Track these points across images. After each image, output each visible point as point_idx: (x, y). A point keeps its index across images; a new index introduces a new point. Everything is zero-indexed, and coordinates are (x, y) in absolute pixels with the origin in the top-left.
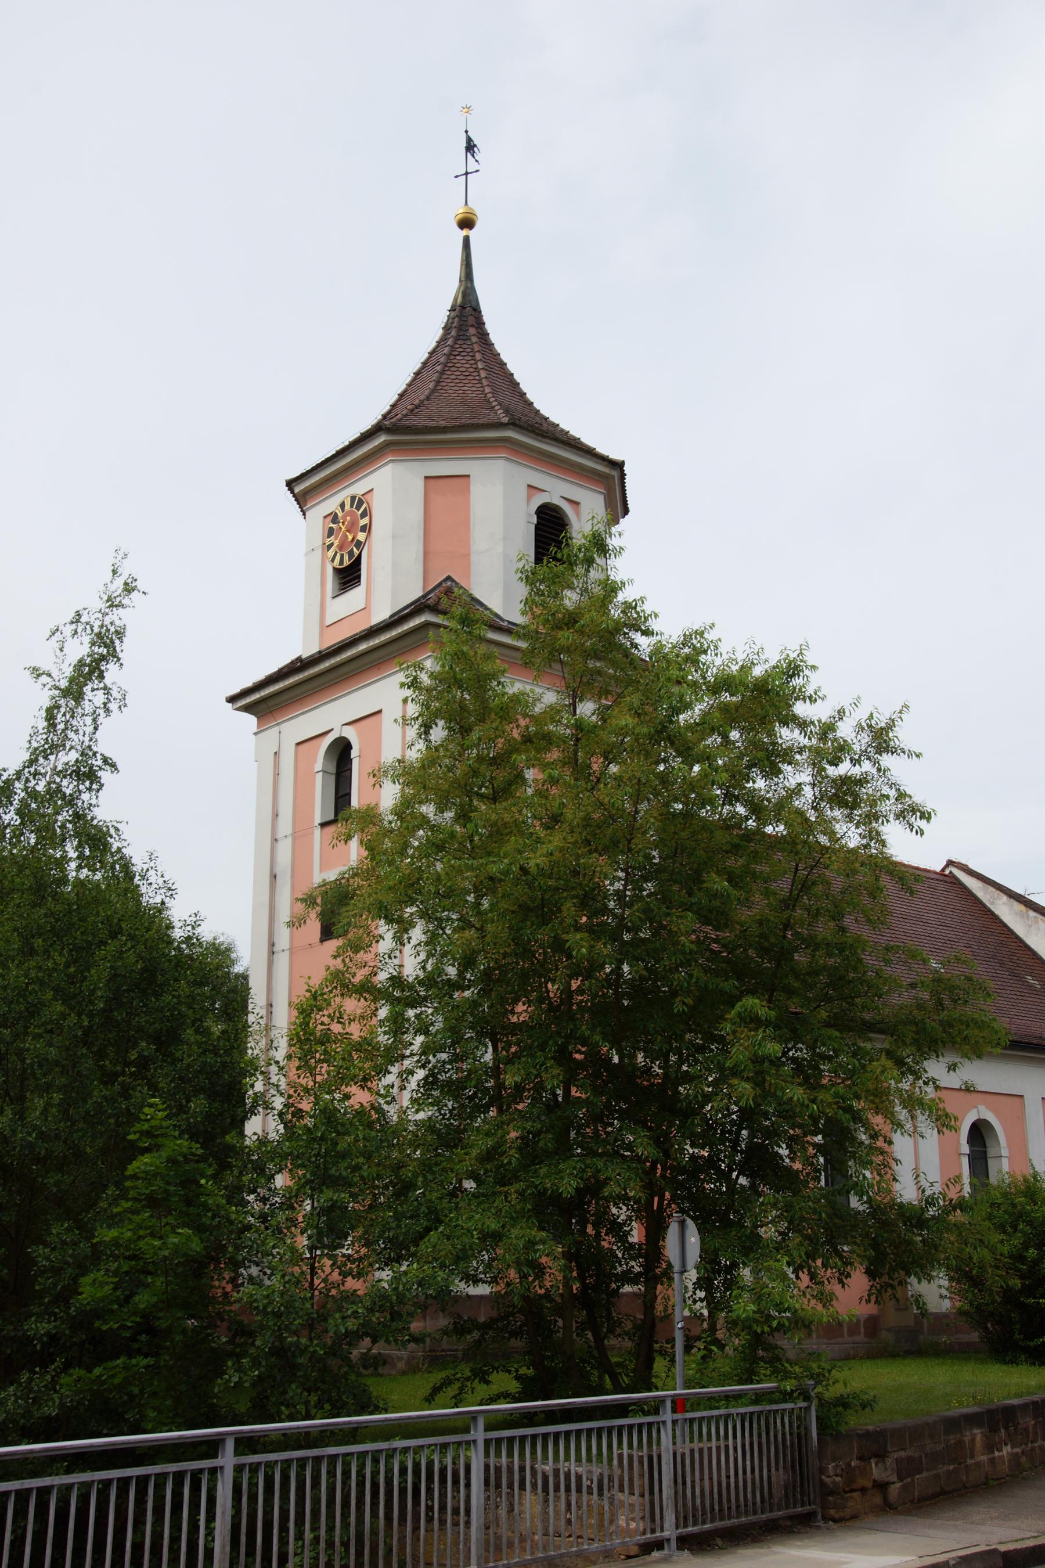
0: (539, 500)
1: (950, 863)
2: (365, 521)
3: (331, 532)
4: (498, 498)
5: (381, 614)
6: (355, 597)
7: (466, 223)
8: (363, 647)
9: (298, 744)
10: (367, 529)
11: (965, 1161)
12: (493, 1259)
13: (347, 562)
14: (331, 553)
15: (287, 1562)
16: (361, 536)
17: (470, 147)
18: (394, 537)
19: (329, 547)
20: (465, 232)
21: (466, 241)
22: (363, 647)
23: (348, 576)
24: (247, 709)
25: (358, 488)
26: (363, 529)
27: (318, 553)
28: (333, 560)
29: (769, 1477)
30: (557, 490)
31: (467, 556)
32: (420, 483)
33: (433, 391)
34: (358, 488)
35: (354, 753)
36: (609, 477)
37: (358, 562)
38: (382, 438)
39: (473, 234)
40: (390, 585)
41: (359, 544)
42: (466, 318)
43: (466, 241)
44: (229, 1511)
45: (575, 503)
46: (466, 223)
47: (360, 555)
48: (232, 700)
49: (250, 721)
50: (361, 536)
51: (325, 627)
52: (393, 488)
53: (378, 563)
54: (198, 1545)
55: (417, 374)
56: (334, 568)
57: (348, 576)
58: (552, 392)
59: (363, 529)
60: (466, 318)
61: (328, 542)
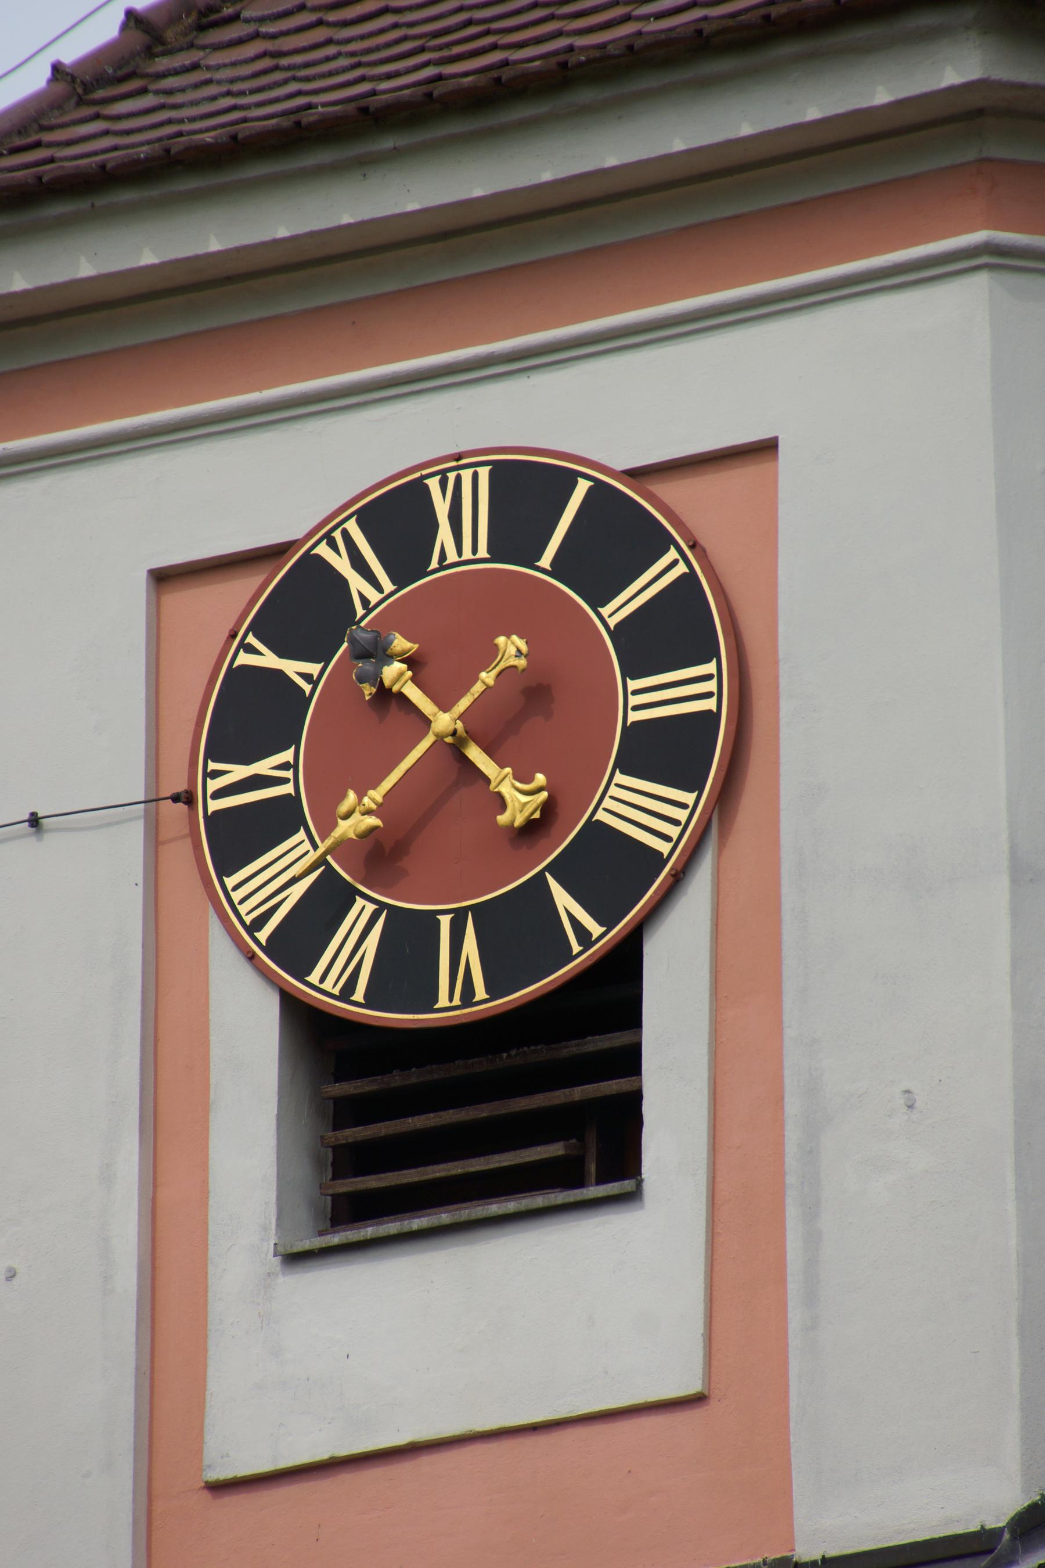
2: (682, 692)
3: (251, 715)
6: (537, 1314)
9: (163, 578)
13: (462, 984)
14: (279, 877)
16: (638, 808)
18: (1022, 873)
19: (241, 836)
25: (610, 407)
26: (668, 751)
27: (107, 873)
28: (299, 940)
34: (610, 407)
41: (614, 870)
44: (242, 57)
47: (623, 965)
50: (638, 808)
54: (146, 412)
56: (310, 1028)
59: (668, 751)
61: (227, 784)
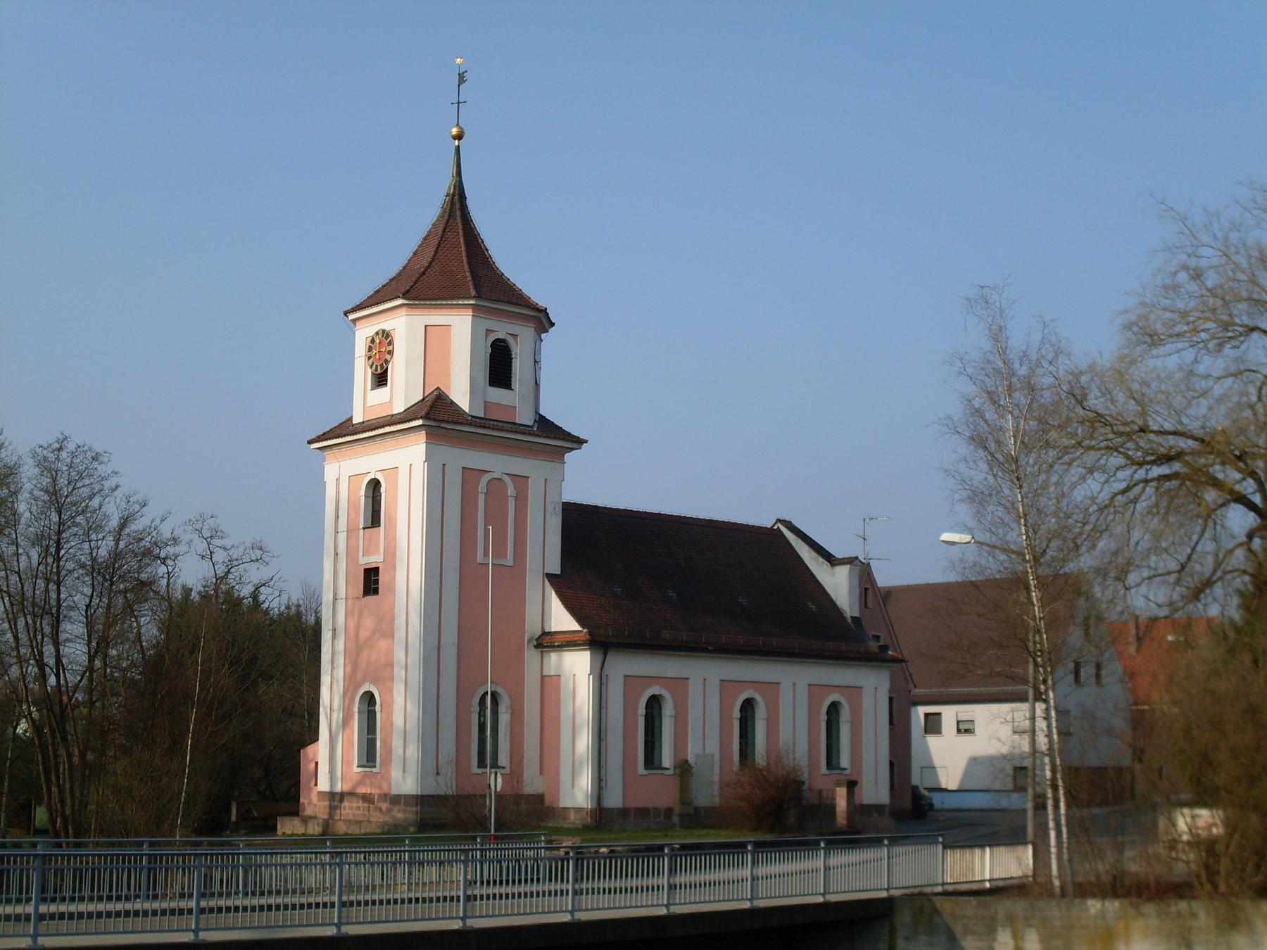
0: (492, 338)
1: (779, 521)
2: (390, 348)
5: (399, 408)
6: (383, 392)
10: (391, 353)
13: (379, 371)
15: (314, 738)
16: (388, 357)
20: (457, 143)
21: (458, 148)
29: (74, 882)
30: (502, 329)
35: (383, 490)
36: (541, 321)
42: (457, 203)
43: (458, 148)
45: (515, 336)
50: (388, 357)
53: (398, 370)
55: (425, 239)
58: (508, 259)
60: (457, 203)
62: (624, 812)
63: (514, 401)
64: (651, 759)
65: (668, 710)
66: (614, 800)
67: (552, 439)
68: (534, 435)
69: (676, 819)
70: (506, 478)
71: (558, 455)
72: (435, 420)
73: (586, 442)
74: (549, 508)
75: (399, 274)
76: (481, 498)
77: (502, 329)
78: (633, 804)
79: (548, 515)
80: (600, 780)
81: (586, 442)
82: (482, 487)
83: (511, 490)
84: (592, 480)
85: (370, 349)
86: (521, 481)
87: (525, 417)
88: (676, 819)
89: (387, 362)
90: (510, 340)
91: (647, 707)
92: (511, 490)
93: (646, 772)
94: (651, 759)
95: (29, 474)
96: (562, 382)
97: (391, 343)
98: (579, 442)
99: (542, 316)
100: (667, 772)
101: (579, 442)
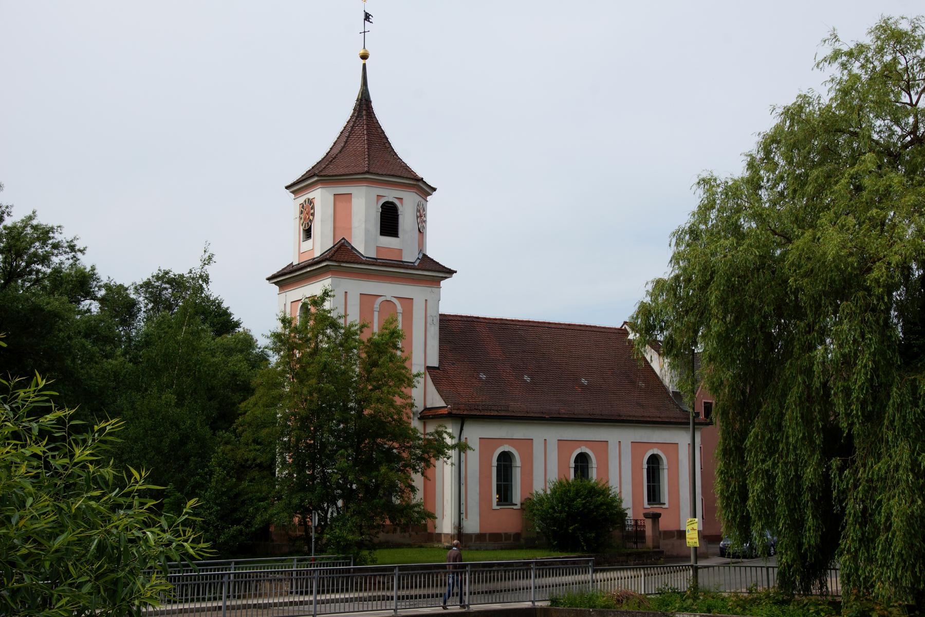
4: (364, 204)
5: (317, 254)
6: (310, 241)
7: (364, 57)
8: (309, 269)
10: (313, 214)
11: (572, 471)
12: (402, 471)
16: (311, 217)
17: (367, 17)
20: (363, 61)
21: (364, 65)
22: (309, 269)
23: (308, 233)
24: (275, 283)
25: (310, 196)
30: (390, 195)
31: (351, 229)
32: (332, 197)
33: (343, 147)
36: (424, 189)
37: (310, 228)
38: (316, 179)
39: (367, 61)
40: (320, 245)
42: (364, 104)
43: (364, 65)
45: (400, 199)
46: (364, 57)
48: (269, 279)
49: (277, 287)
50: (311, 217)
51: (300, 254)
52: (321, 196)
57: (308, 233)
60: (364, 104)
62: (480, 537)
63: (402, 246)
64: (505, 494)
65: (518, 461)
66: (472, 526)
67: (433, 272)
68: (417, 269)
69: (523, 541)
70: (394, 300)
71: (435, 282)
72: (335, 261)
73: (456, 272)
74: (429, 320)
75: (323, 159)
76: (376, 314)
77: (390, 195)
78: (489, 530)
79: (428, 325)
80: (460, 513)
81: (456, 272)
82: (377, 306)
83: (399, 308)
84: (454, 299)
85: (302, 212)
86: (407, 302)
87: (410, 256)
88: (523, 541)
89: (311, 221)
90: (397, 202)
91: (498, 461)
92: (399, 308)
93: (498, 508)
94: (505, 494)
95: (142, 300)
96: (444, 232)
97: (313, 208)
98: (451, 272)
99: (421, 184)
100: (515, 507)
101: (451, 272)
